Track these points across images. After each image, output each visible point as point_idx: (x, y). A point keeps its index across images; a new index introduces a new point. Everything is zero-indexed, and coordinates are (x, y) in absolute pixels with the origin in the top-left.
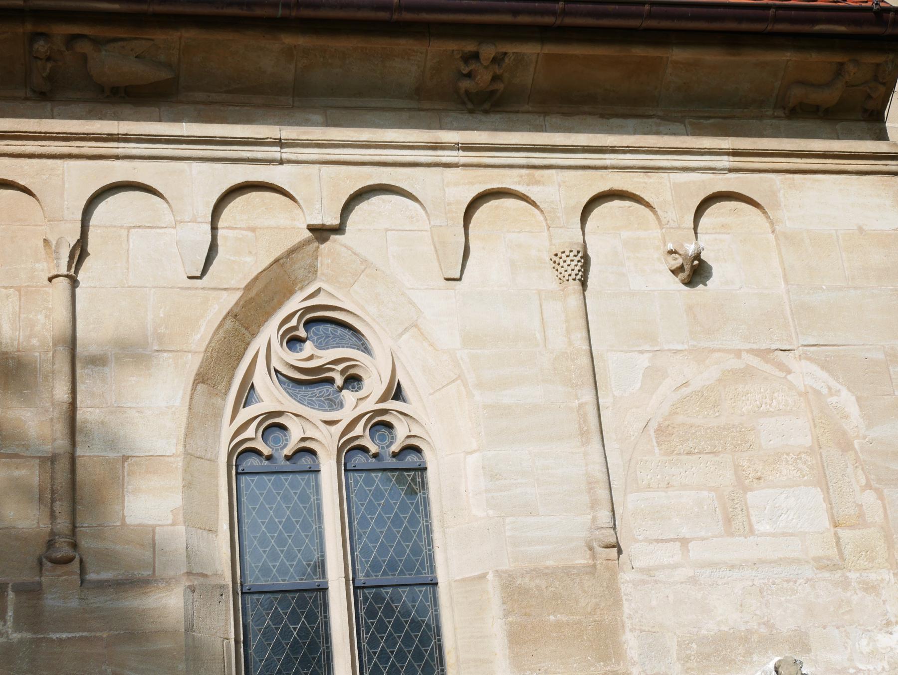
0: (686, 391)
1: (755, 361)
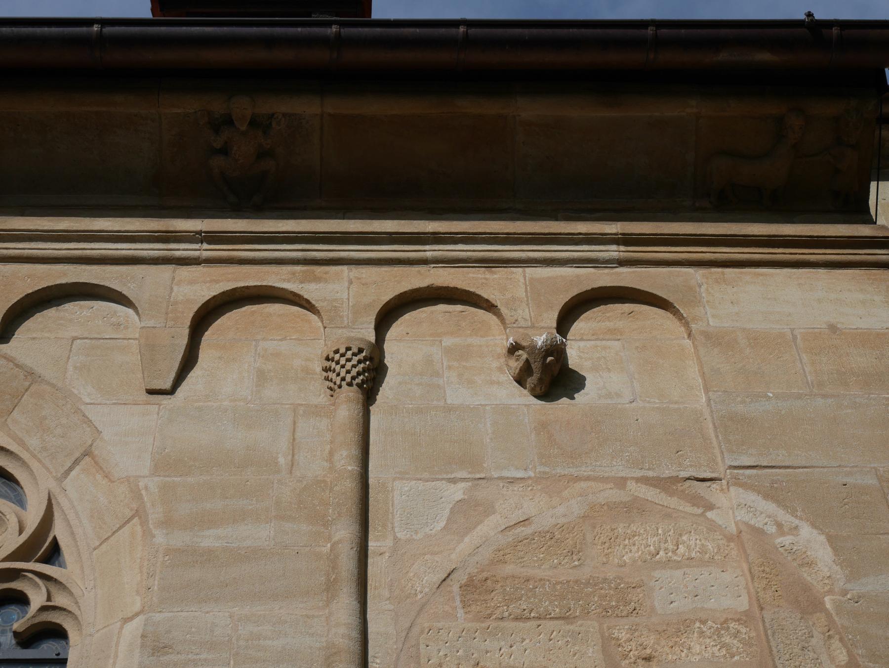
0: (527, 530)
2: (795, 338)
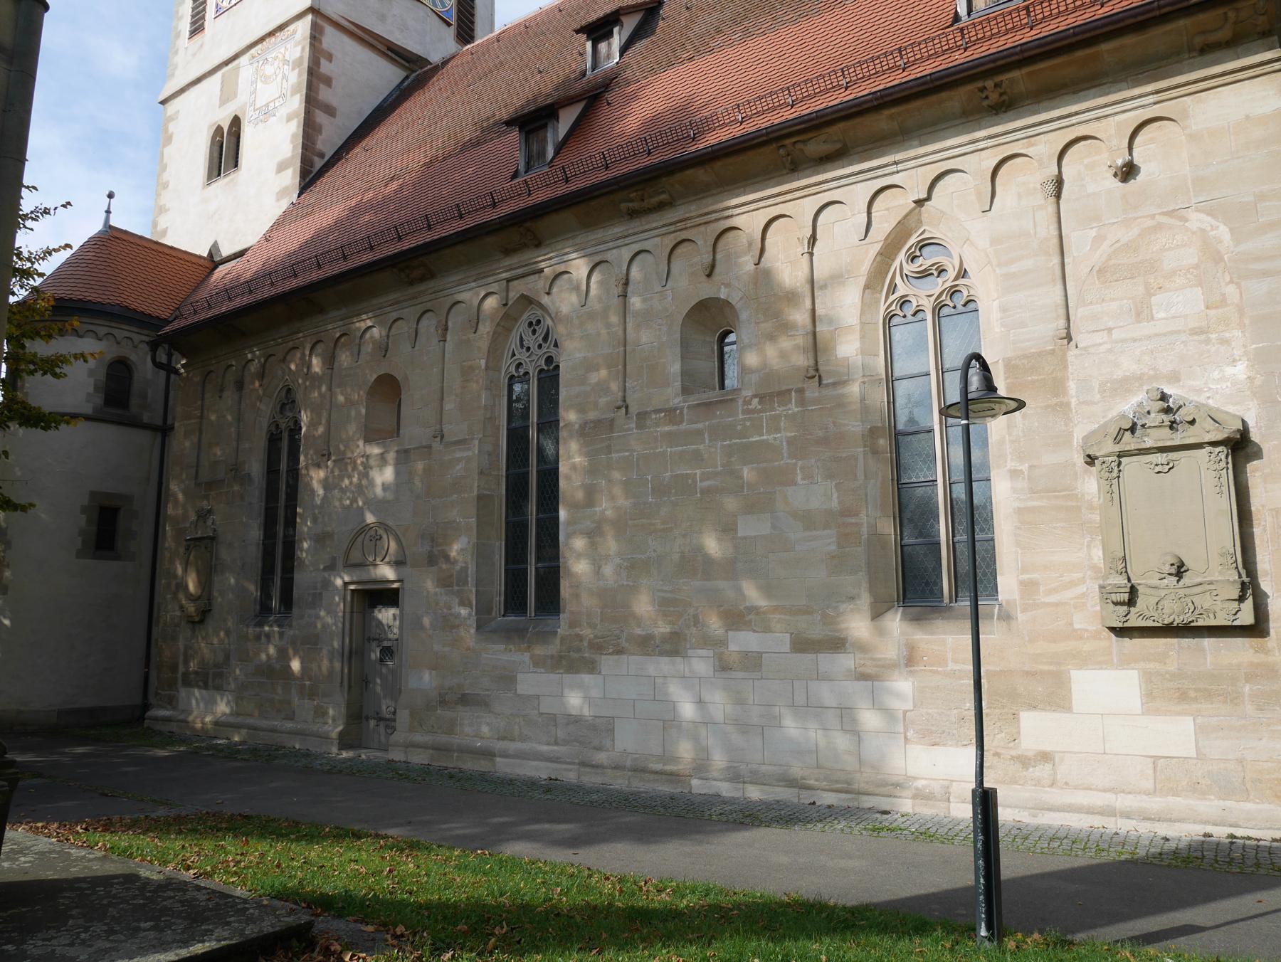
0: (1118, 245)
1: (1164, 219)
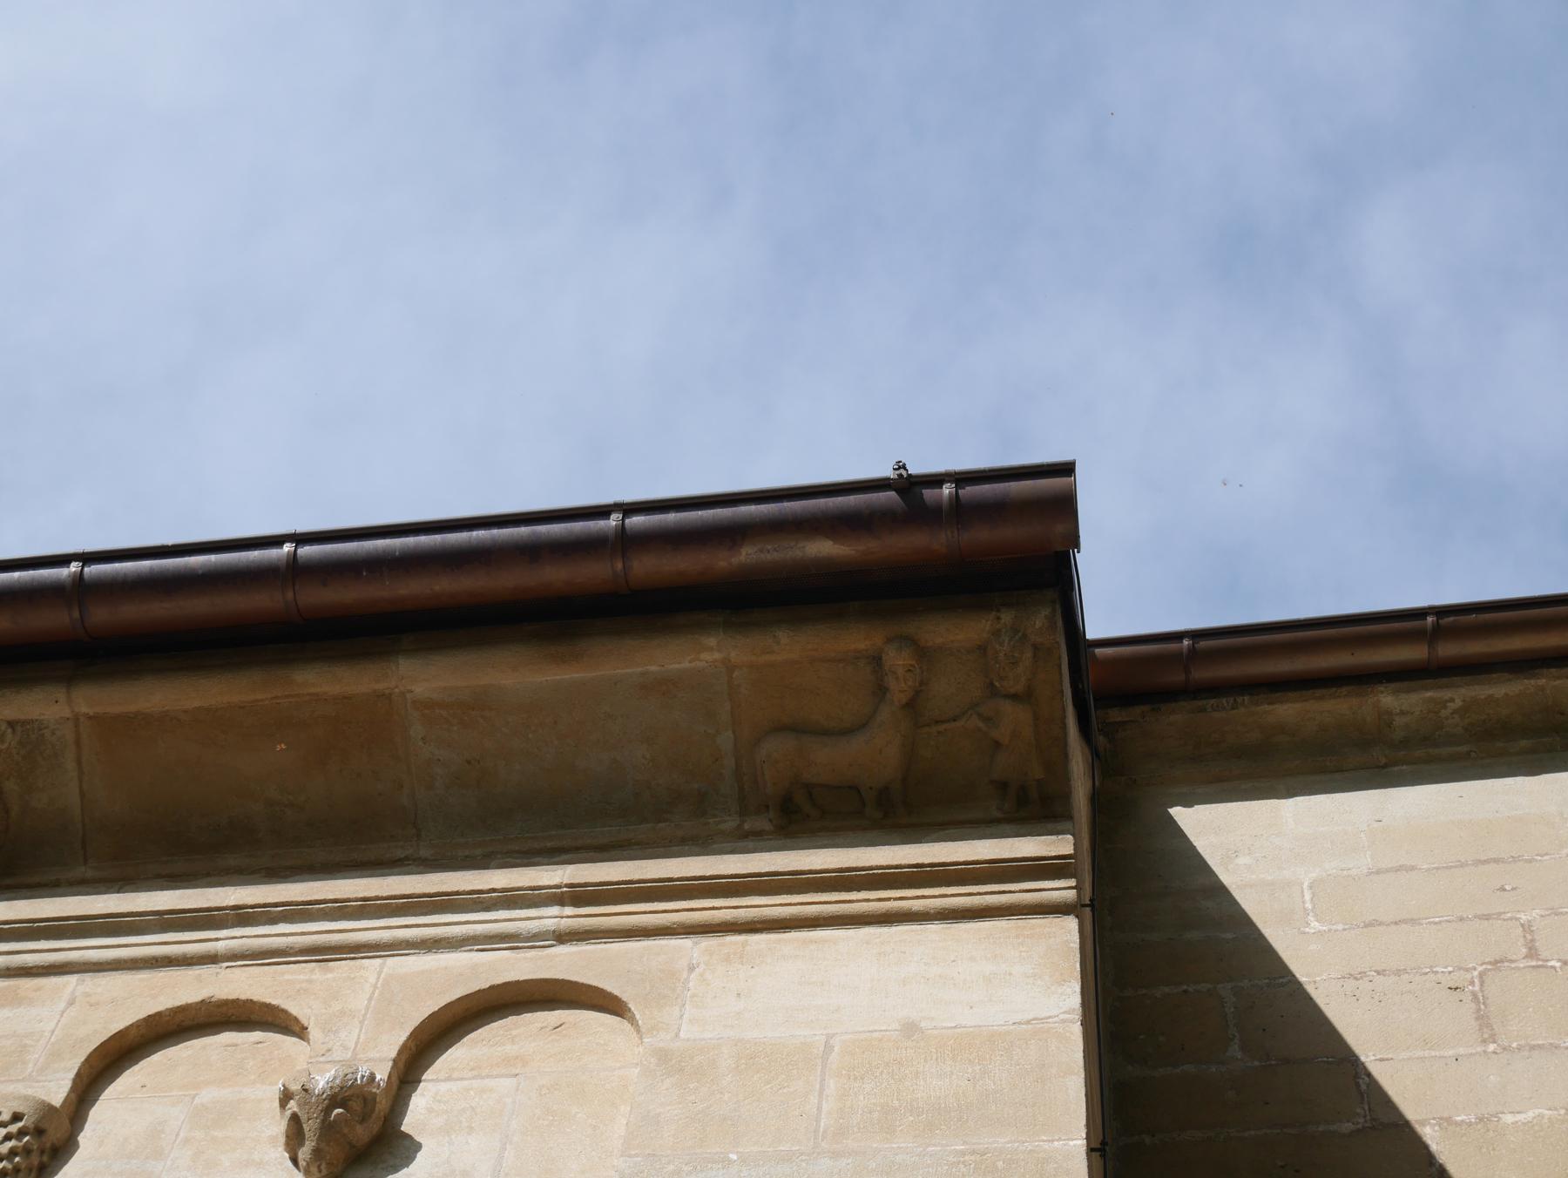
2: (828, 1048)
